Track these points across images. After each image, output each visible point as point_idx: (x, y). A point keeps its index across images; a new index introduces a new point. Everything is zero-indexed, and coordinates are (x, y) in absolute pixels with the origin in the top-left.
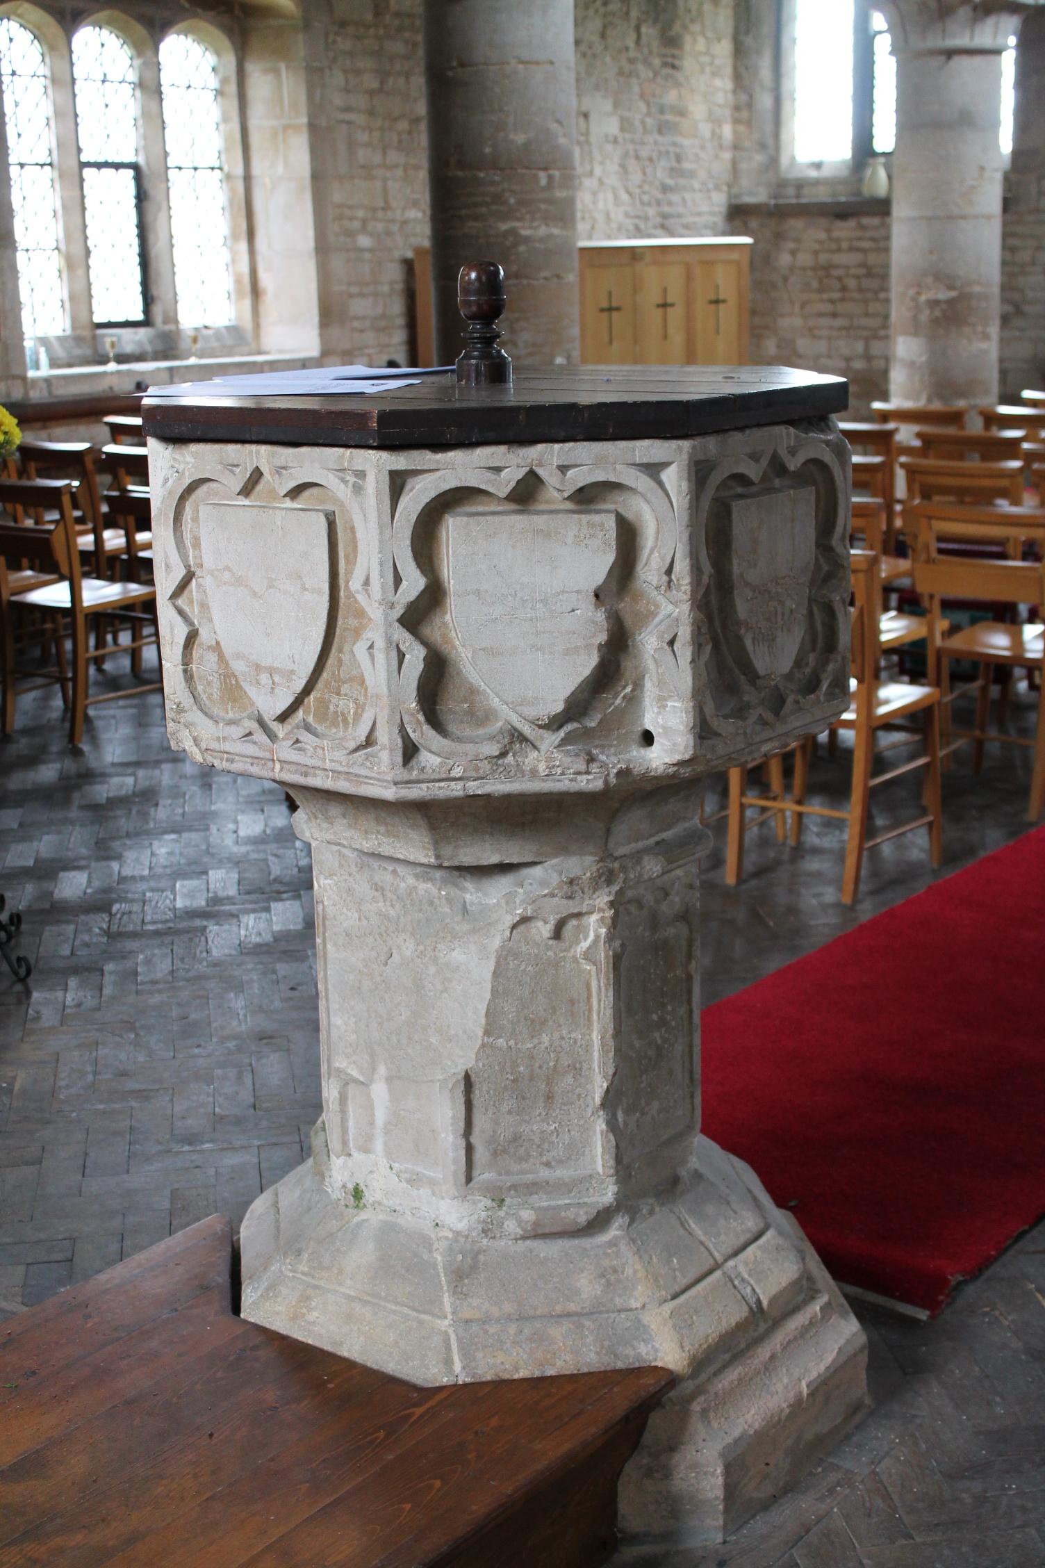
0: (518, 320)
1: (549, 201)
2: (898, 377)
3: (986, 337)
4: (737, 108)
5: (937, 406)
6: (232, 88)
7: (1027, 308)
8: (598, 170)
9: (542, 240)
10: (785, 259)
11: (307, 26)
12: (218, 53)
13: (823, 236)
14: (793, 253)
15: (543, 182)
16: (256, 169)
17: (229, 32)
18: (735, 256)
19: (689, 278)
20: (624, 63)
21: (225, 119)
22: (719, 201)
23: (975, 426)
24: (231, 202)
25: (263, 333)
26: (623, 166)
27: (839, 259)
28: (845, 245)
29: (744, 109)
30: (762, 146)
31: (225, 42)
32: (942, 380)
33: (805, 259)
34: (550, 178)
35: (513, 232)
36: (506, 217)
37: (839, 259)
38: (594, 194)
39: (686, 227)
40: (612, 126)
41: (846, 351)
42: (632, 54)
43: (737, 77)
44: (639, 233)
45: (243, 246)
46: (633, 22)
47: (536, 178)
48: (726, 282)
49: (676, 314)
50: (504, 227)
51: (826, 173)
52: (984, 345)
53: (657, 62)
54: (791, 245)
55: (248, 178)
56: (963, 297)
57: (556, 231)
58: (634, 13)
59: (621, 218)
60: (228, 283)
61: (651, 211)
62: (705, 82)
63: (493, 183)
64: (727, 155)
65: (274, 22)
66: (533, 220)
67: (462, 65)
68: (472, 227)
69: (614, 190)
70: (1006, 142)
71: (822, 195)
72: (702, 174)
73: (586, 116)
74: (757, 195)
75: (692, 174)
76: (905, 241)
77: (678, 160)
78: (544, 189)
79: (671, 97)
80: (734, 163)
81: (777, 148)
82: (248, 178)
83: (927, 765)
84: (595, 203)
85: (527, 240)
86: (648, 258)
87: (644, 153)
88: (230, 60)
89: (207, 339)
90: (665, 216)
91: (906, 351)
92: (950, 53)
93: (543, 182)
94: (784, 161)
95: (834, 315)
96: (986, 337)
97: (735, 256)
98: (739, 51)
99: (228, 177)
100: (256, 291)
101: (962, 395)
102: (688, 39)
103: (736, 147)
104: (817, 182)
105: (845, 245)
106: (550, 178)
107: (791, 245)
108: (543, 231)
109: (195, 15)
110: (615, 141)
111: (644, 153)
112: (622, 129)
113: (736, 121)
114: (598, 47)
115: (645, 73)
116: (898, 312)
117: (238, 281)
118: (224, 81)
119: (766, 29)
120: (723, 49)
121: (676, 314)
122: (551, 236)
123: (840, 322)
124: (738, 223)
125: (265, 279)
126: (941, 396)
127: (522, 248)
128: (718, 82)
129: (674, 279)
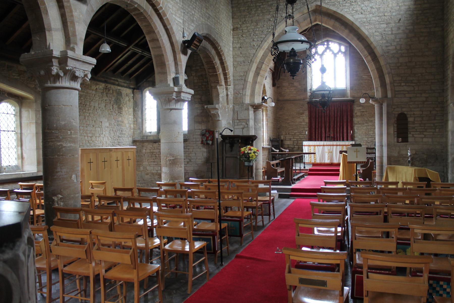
0: (63, 166)
1: (71, 138)
2: (163, 176)
3: (181, 167)
4: (134, 121)
5: (171, 182)
6: (18, 114)
7: (192, 160)
8: (104, 133)
9: (68, 147)
10: (144, 151)
11: (36, 101)
12: (15, 107)
13: (151, 146)
14: (146, 150)
15: (69, 133)
16: (23, 132)
17: (18, 102)
18: (133, 150)
19: (123, 155)
20: (110, 112)
21: (16, 121)
22: (131, 139)
23: (178, 188)
24: (17, 138)
25: (24, 167)
26: (109, 132)
27: (154, 151)
28: (156, 148)
29: (135, 121)
30: (139, 129)
31: (17, 104)
32: (172, 177)
33: (148, 151)
34: (71, 132)
35: (61, 145)
36: (59, 141)
37: (154, 151)
38: (103, 138)
39: (124, 145)
40: (107, 124)
41: (157, 169)
42: (111, 110)
43: (134, 116)
44: (113, 146)
45: (20, 148)
46: (112, 104)
47: (67, 132)
48: (131, 155)
49: (120, 162)
50: (59, 144)
51: (152, 134)
52: (181, 169)
53: (117, 112)
54: (145, 148)
55: (21, 133)
56: (176, 159)
57: (72, 145)
58: (112, 102)
59: (109, 142)
60: (16, 156)
61: (116, 141)
62: (127, 117)
63: (56, 133)
64: (132, 131)
65: (28, 101)
66: (66, 142)
67: (49, 106)
68: (51, 144)
69: (108, 137)
70: (185, 127)
71: (151, 138)
72: (127, 134)
73: (101, 122)
74: (138, 138)
75: (125, 134)
76: (163, 147)
77: (122, 131)
78: (69, 135)
79: (120, 119)
80: (134, 132)
81: (143, 129)
82: (21, 133)
83: (158, 286)
84: (103, 139)
85: (65, 147)
86: (113, 151)
87: (114, 130)
88: (18, 108)
89: (9, 168)
90: (119, 142)
91: (165, 170)
92: (171, 109)
93: (69, 133)
94: (144, 132)
95: (154, 162)
96: (181, 167)
97: (133, 150)
98: (134, 110)
99: (17, 133)
100: (22, 158)
101: (177, 179)
102: (123, 108)
103: (134, 129)
104: (150, 136)
105: (156, 148)
106: (71, 132)
107: (145, 148)
108: (69, 145)
109: (9, 99)
110: (108, 127)
111: (114, 130)
112: (109, 125)
113: (134, 124)
114: (104, 109)
115: (114, 114)
116: (163, 162)
117: (18, 155)
118: (16, 113)
119: (140, 107)
120: (131, 110)
121: (120, 162)
122: (71, 146)
123: (155, 163)
124: (134, 144)
125: (25, 155)
126: (172, 180)
127: (64, 149)
128: (130, 116)
129: (119, 155)
